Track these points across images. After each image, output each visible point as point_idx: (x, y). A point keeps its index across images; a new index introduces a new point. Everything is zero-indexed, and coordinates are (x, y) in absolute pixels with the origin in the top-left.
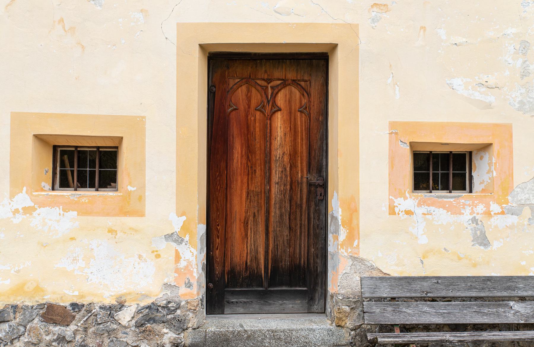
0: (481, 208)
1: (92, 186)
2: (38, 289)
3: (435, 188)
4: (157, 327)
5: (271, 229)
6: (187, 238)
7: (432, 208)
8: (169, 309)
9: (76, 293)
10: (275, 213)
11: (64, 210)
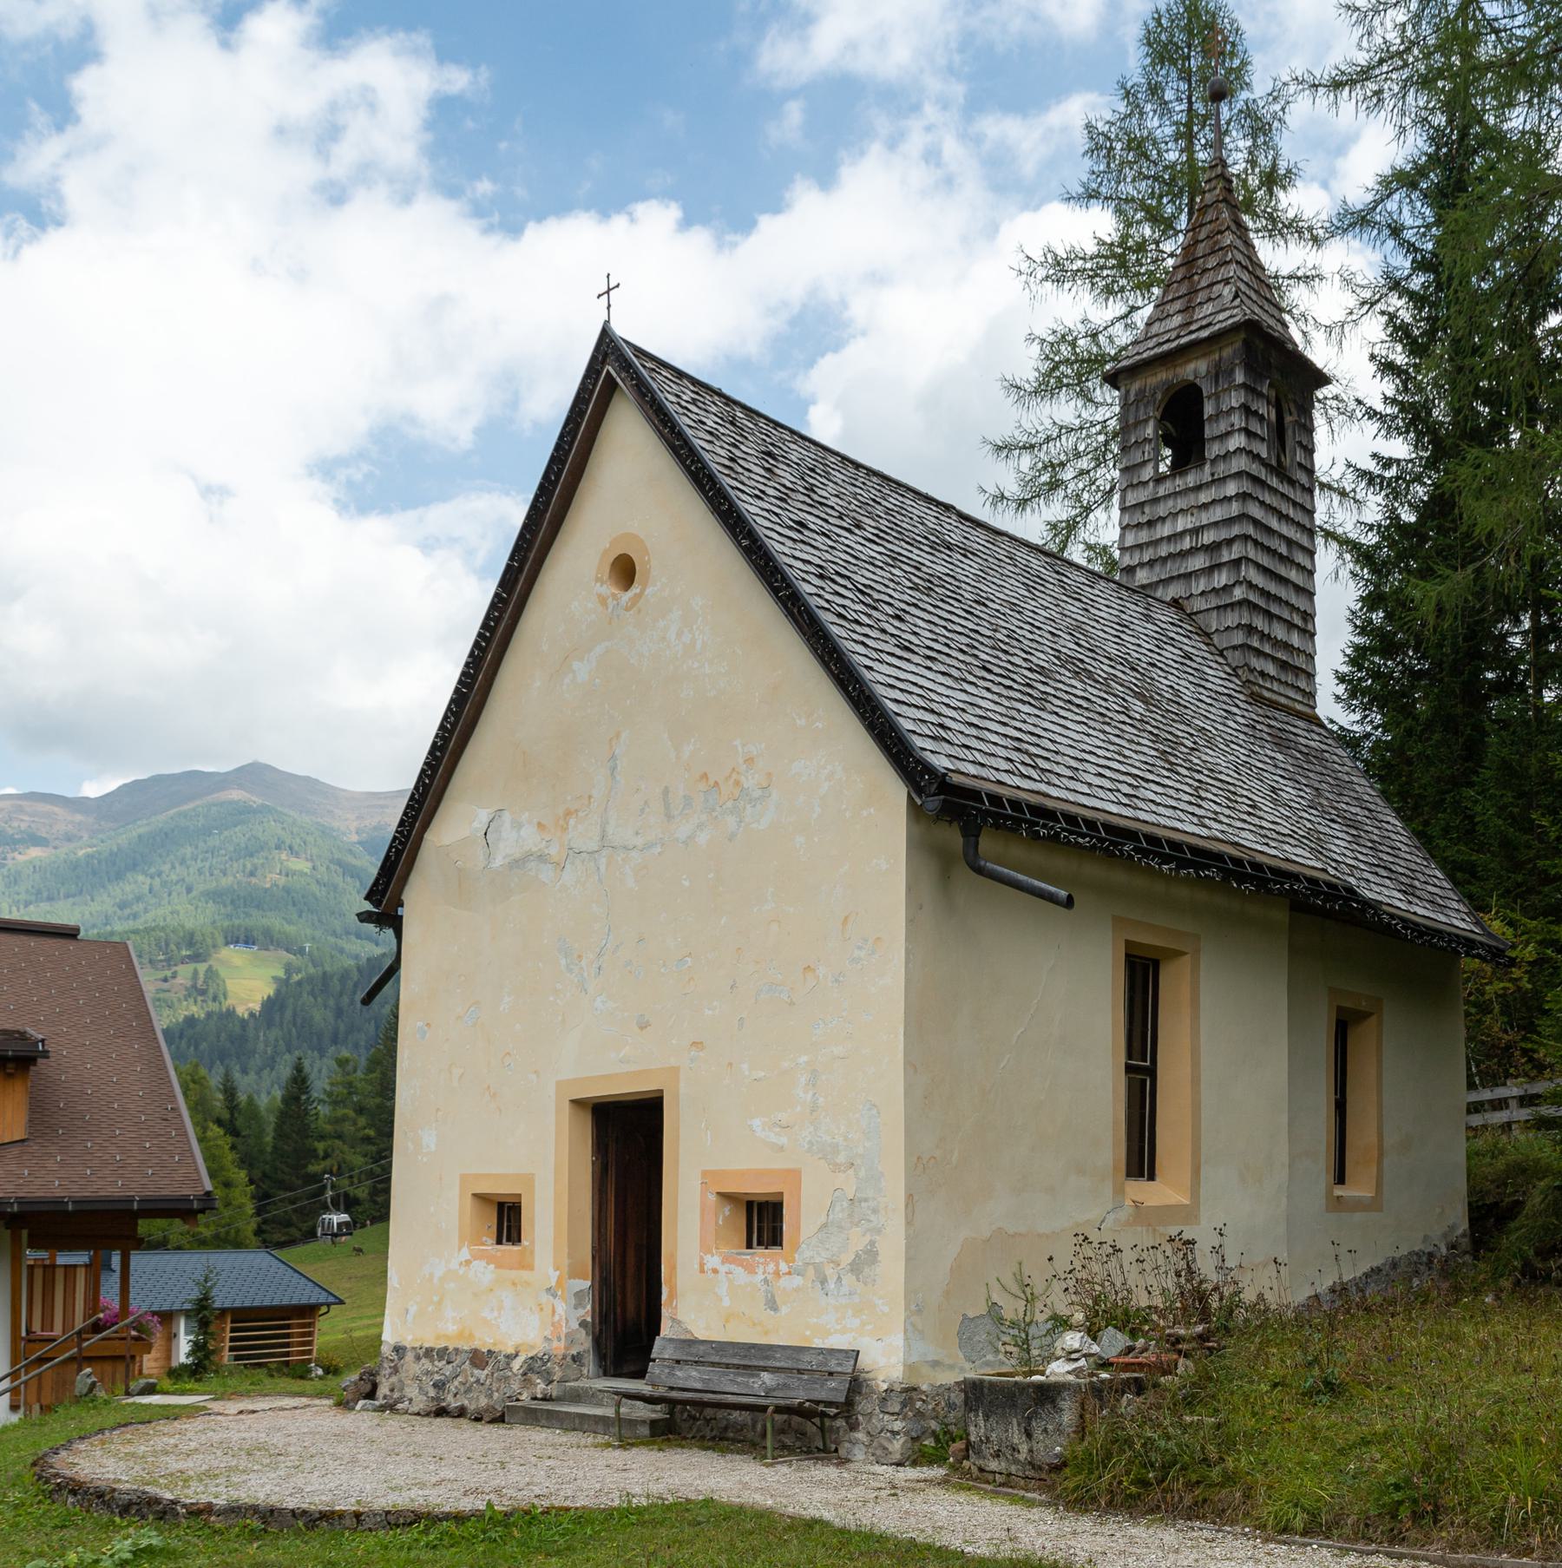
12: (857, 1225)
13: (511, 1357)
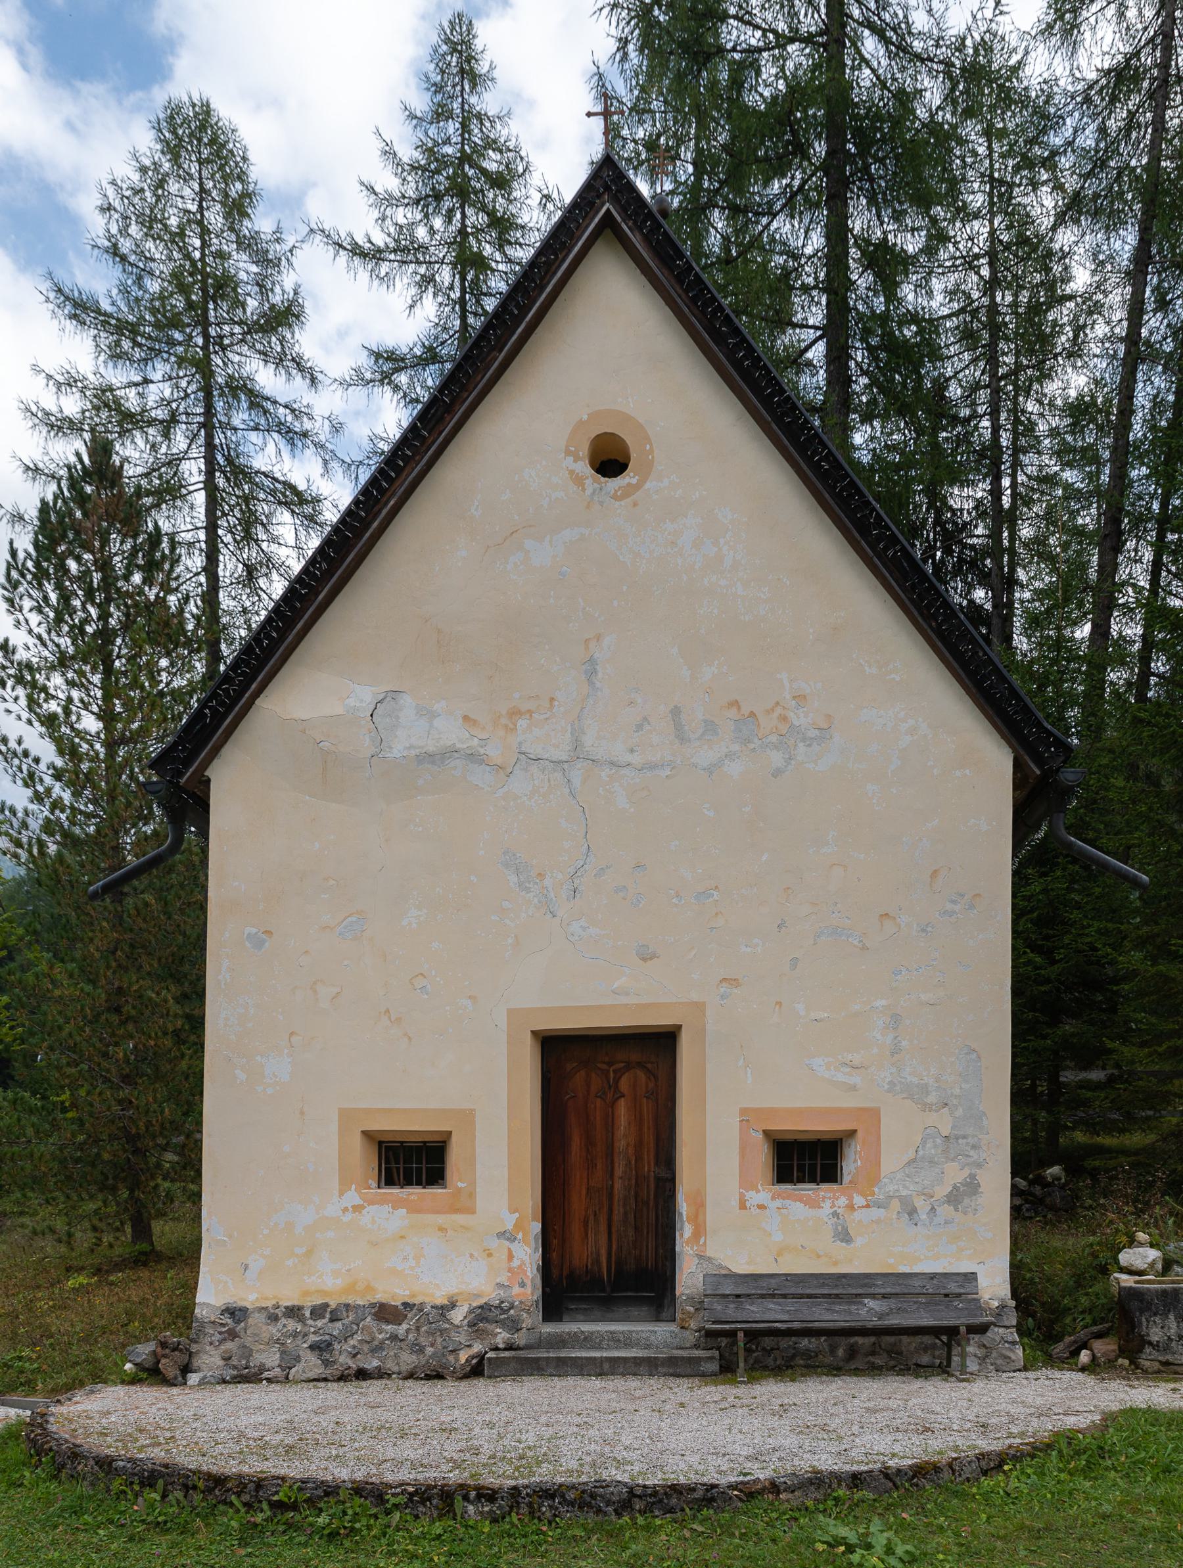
0: (843, 1201)
1: (419, 1183)
2: (369, 1288)
3: (801, 1180)
4: (490, 1327)
5: (614, 1229)
6: (520, 1236)
7: (788, 1202)
8: (502, 1309)
9: (407, 1292)
10: (618, 1211)
11: (393, 1208)
12: (953, 1160)
13: (443, 1311)
